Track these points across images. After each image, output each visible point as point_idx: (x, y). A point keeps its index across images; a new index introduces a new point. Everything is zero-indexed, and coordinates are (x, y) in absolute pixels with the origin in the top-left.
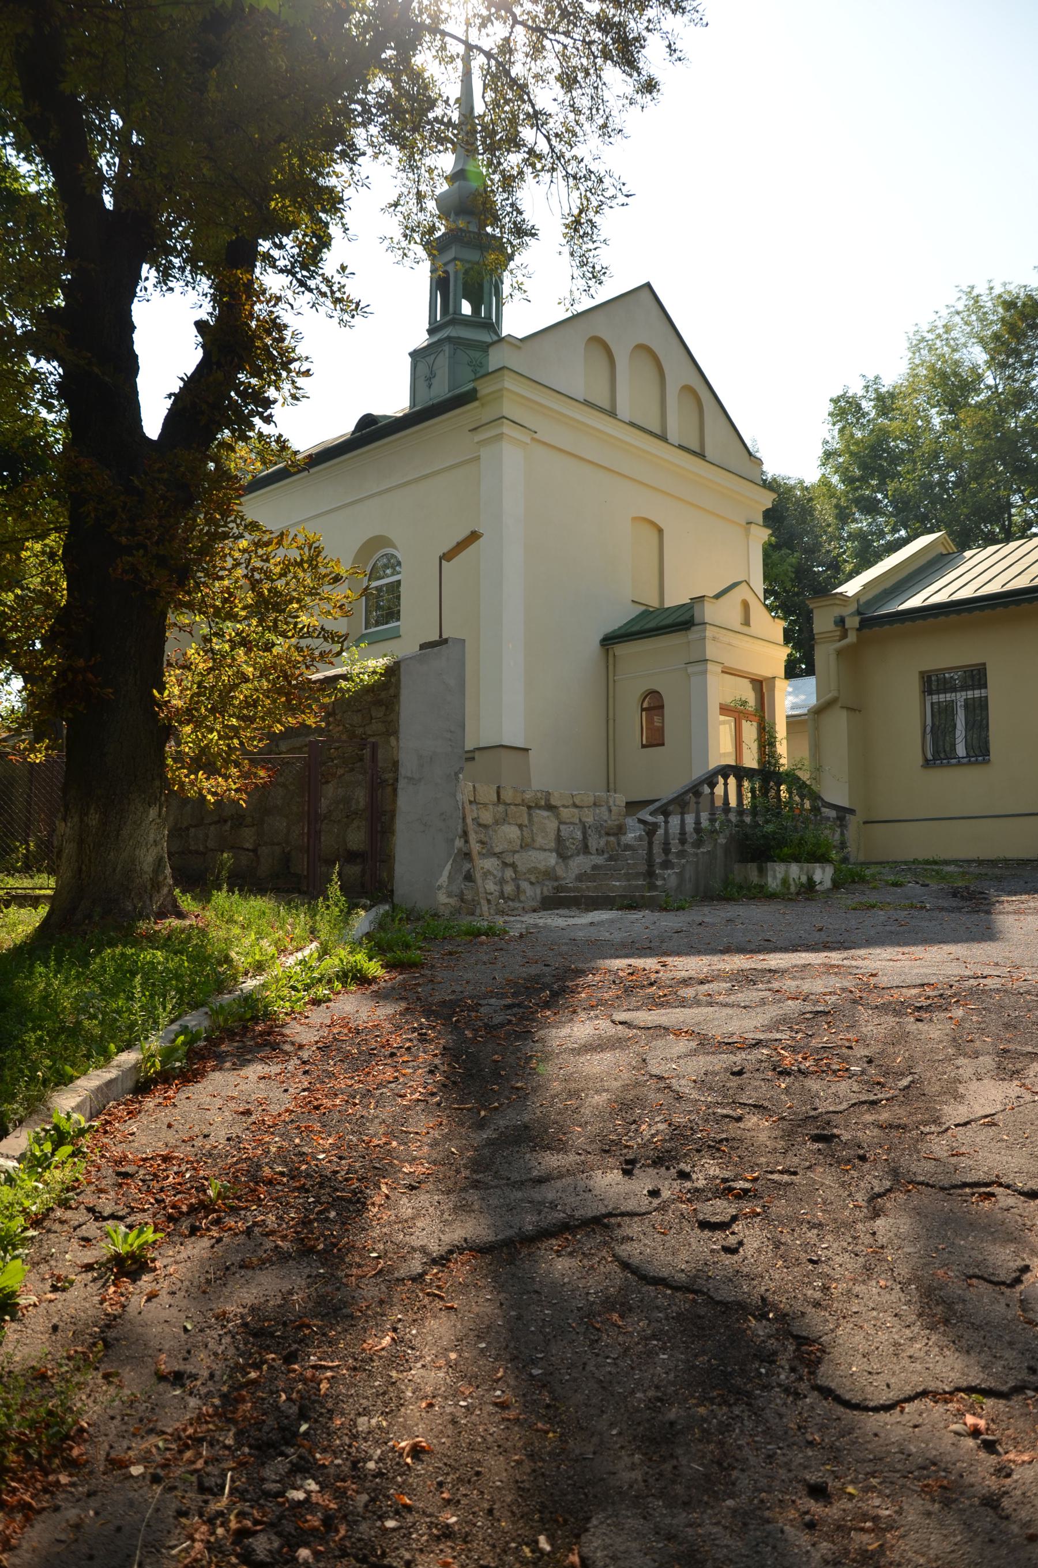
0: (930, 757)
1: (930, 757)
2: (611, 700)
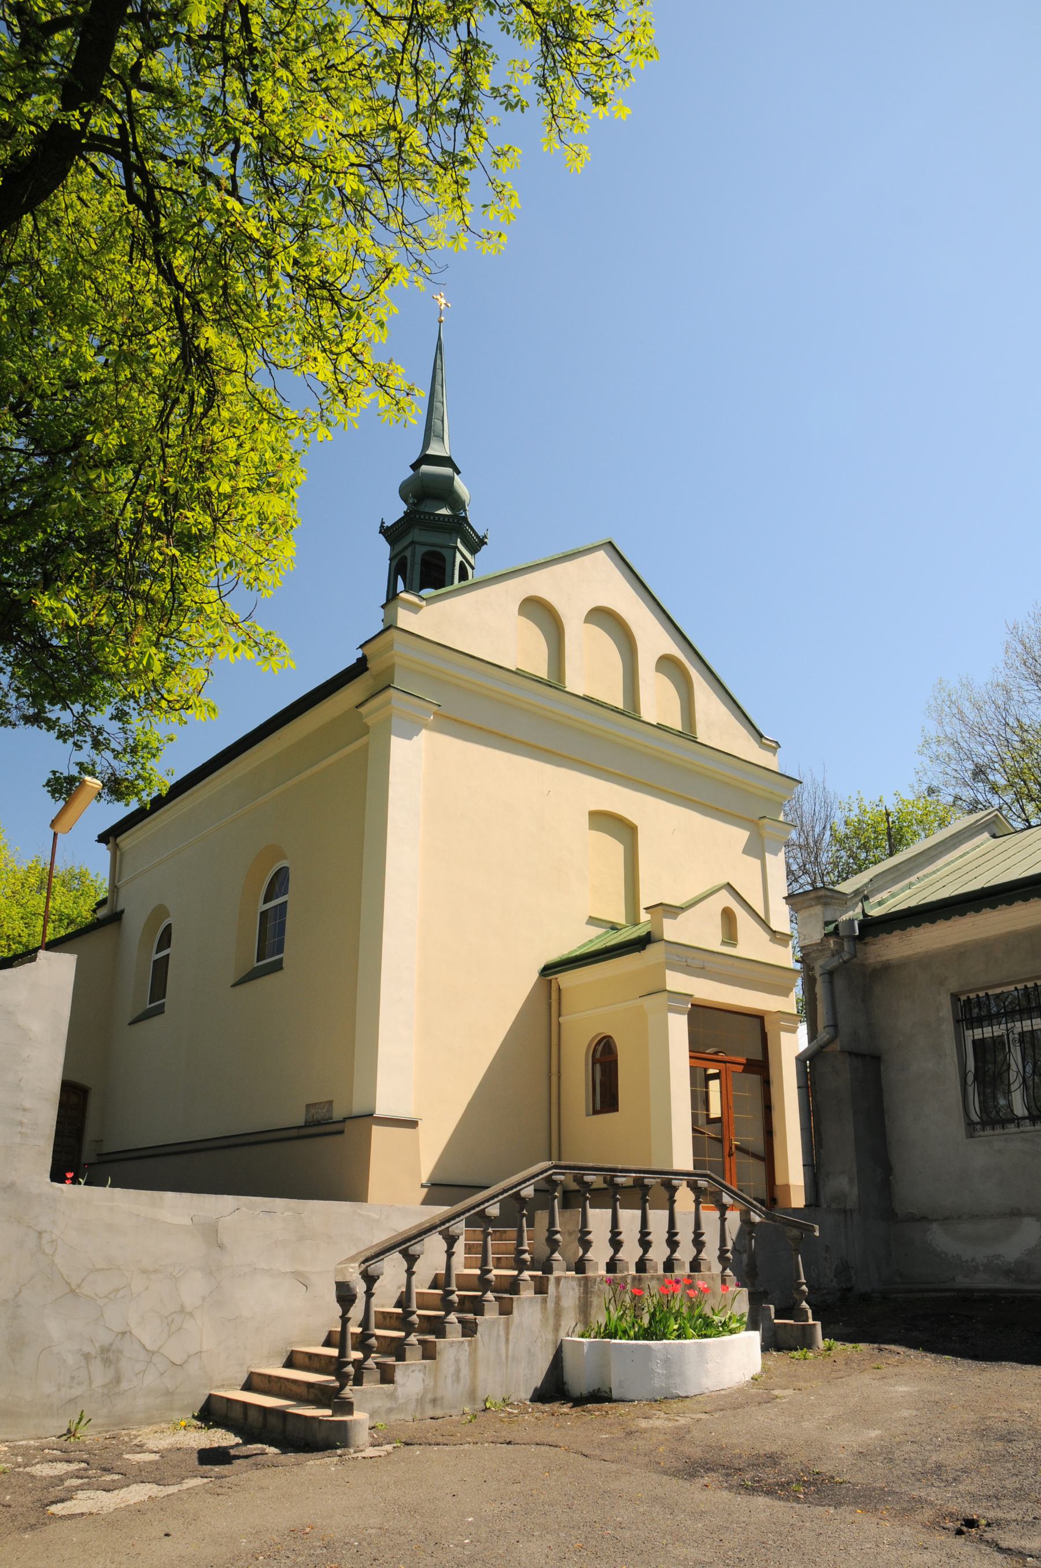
0: (975, 1118)
1: (975, 1118)
2: (554, 1079)
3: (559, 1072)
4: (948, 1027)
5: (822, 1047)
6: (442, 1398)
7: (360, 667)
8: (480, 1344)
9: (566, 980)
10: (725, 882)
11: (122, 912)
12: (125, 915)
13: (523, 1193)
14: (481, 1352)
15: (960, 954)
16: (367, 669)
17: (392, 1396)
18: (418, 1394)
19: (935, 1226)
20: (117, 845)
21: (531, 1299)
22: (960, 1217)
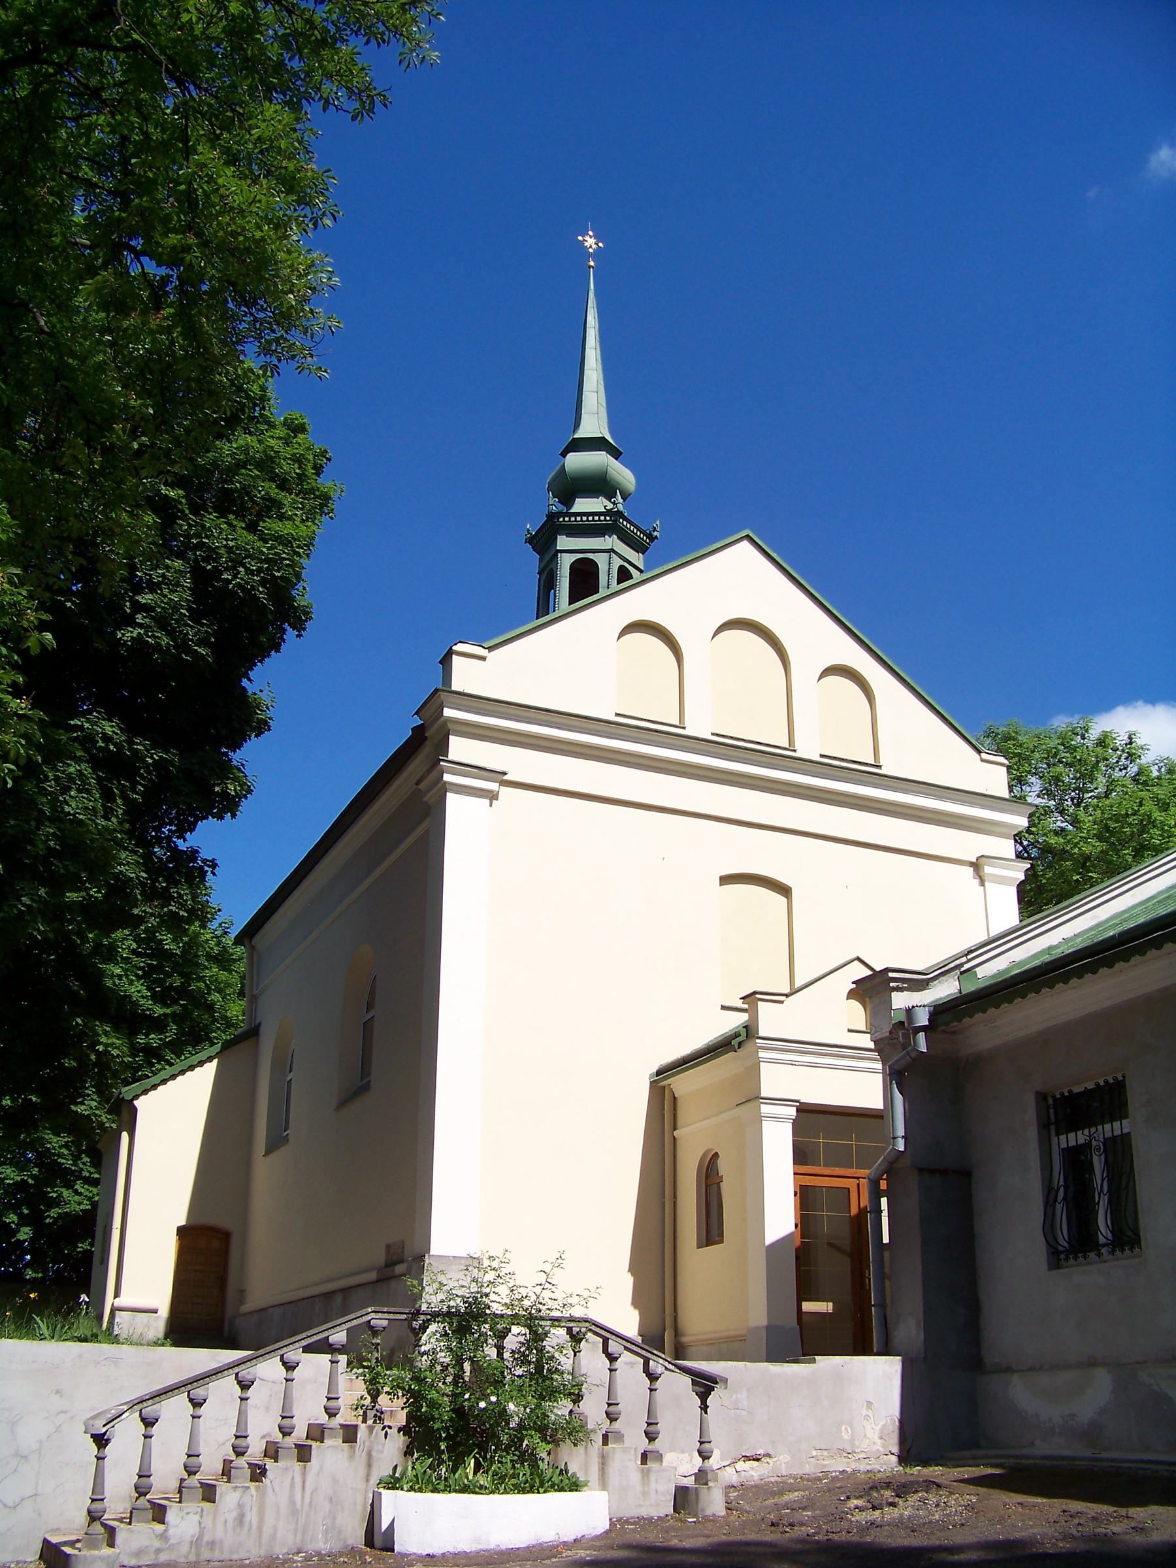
3: (675, 1197)
4: (1032, 1133)
5: (892, 1164)
6: (221, 1541)
7: (419, 731)
8: (270, 1491)
9: (681, 1084)
10: (855, 956)
11: (260, 1024)
12: (262, 1028)
13: (332, 1339)
14: (270, 1498)
15: (1044, 1041)
16: (426, 738)
17: (163, 1536)
18: (193, 1536)
19: (1016, 1378)
20: (253, 947)
21: (336, 1447)
22: (1041, 1368)
